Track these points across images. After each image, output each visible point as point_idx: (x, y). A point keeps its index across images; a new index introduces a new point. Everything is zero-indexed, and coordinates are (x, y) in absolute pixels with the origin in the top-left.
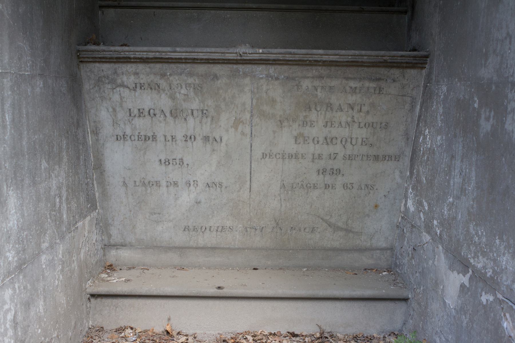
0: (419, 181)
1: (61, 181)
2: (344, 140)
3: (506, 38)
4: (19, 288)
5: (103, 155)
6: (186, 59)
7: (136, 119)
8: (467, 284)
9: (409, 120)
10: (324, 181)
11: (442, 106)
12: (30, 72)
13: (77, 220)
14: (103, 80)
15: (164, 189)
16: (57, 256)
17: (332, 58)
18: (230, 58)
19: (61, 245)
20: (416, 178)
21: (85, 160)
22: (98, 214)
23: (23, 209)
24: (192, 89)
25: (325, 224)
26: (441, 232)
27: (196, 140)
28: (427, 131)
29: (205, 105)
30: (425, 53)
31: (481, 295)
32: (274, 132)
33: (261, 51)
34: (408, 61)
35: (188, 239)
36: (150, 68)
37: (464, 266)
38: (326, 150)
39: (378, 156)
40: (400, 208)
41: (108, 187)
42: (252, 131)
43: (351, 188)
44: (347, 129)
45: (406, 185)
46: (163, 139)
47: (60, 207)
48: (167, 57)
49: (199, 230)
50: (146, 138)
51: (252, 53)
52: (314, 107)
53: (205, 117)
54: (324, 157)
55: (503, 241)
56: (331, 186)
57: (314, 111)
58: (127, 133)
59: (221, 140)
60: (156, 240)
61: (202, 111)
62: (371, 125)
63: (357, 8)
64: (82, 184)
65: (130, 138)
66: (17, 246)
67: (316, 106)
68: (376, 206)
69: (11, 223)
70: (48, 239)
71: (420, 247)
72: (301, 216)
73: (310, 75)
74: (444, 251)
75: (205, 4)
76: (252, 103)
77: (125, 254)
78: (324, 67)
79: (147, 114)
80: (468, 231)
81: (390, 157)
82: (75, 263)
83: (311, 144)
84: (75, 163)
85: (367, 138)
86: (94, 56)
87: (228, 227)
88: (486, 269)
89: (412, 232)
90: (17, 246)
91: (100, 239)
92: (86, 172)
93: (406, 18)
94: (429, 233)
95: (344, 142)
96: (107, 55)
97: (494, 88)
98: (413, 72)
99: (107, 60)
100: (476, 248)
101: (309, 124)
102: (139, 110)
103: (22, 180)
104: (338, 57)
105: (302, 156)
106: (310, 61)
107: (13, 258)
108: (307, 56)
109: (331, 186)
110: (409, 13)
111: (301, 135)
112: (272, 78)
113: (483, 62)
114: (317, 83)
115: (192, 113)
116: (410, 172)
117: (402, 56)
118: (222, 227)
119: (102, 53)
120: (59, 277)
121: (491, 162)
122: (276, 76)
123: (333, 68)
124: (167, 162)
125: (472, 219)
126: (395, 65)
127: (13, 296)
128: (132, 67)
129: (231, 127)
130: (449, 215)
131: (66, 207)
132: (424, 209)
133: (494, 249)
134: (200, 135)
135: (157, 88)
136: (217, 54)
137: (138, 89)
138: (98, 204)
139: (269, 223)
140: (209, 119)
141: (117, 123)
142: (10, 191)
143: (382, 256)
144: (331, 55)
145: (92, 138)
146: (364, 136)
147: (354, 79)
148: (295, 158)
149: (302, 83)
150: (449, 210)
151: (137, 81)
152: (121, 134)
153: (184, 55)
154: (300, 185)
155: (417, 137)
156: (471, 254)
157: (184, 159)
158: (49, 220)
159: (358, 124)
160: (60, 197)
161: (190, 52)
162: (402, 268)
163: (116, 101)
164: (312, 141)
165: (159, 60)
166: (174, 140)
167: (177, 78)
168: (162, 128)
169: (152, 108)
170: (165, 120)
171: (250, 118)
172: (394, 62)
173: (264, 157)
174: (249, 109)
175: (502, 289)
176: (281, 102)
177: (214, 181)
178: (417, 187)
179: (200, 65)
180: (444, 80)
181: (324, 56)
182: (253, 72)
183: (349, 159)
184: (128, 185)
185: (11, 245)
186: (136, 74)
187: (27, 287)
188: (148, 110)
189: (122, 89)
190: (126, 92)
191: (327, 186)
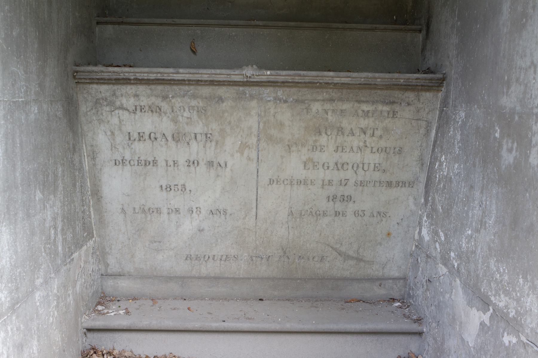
0: (434, 209)
1: (56, 211)
2: (355, 166)
3: (530, 67)
4: (12, 329)
5: (100, 180)
6: (189, 80)
7: (136, 143)
8: (487, 323)
9: (424, 145)
10: (334, 209)
11: (460, 132)
12: (24, 98)
13: (73, 251)
14: (101, 101)
15: (165, 216)
16: (51, 292)
17: (344, 80)
18: (235, 80)
19: (56, 280)
20: (431, 206)
21: (81, 186)
22: (95, 242)
23: (16, 245)
24: (195, 112)
25: (335, 253)
26: (458, 265)
27: (200, 165)
28: (443, 157)
29: (210, 129)
30: (441, 76)
31: (503, 337)
32: (282, 157)
33: (269, 73)
34: (423, 84)
35: (190, 268)
36: (151, 89)
37: (485, 303)
38: (337, 176)
39: (391, 182)
40: (414, 236)
41: (105, 214)
42: (258, 155)
43: (362, 215)
44: (359, 154)
45: (420, 212)
46: (164, 164)
47: (55, 239)
48: (169, 78)
49: (202, 259)
50: (147, 163)
51: (259, 75)
52: (324, 131)
53: (209, 141)
54: (334, 183)
55: (528, 281)
56: (341, 213)
57: (324, 134)
58: (126, 158)
59: (226, 165)
60: (155, 269)
61: (206, 134)
62: (384, 150)
63: (369, 26)
64: (78, 212)
65: (130, 162)
66: (10, 285)
67: (326, 130)
68: (389, 234)
69: (4, 261)
70: (42, 274)
71: (435, 279)
72: (310, 244)
73: (320, 97)
74: (462, 285)
75: (209, 21)
76: (259, 127)
77: (123, 284)
78: (335, 90)
79: (147, 137)
80: (488, 267)
81: (404, 183)
82: (71, 297)
83: (321, 169)
84: (70, 190)
85: (379, 164)
86: (92, 77)
87: (232, 256)
88: (508, 309)
89: (427, 262)
90: (10, 285)
91: (97, 268)
92: (82, 200)
93: (420, 37)
94: (445, 265)
95: (356, 167)
96: (106, 76)
97: (517, 118)
98: (428, 95)
99: (106, 82)
100: (498, 285)
101: (319, 148)
102: (139, 133)
103: (16, 214)
104: (350, 79)
105: (311, 182)
106: (320, 83)
107: (6, 298)
108: (317, 78)
109: (341, 213)
110: (424, 32)
111: (310, 160)
112: (280, 101)
113: (505, 90)
114: (328, 106)
115: (196, 137)
116: (424, 199)
117: (417, 79)
118: (227, 256)
119: (100, 74)
120: (54, 314)
121: (513, 196)
122: (284, 99)
123: (345, 91)
124: (169, 188)
125: (493, 254)
126: (410, 87)
127: (6, 339)
128: (131, 89)
129: (237, 152)
130: (468, 248)
131: (61, 238)
132: (440, 239)
133: (518, 289)
134: (203, 159)
135: (158, 111)
136: (222, 76)
137: (138, 112)
138: (95, 232)
139: (276, 252)
140: (214, 143)
141: (115, 147)
142: (3, 228)
143: (395, 286)
144: (343, 78)
145: (88, 163)
146: (377, 162)
147: (367, 102)
148: (304, 184)
149: (312, 106)
150: (468, 243)
151: (137, 103)
152: (120, 159)
153: (187, 77)
154: (308, 213)
155: (432, 164)
156: (491, 291)
157: (187, 185)
158: (43, 254)
159: (370, 149)
160: (55, 228)
161: (193, 74)
162: (416, 299)
163: (115, 124)
164: (321, 166)
165: (161, 82)
166: (176, 165)
167: (179, 100)
168: (163, 152)
169: (153, 131)
170: (166, 144)
171: (257, 142)
172: (409, 85)
173: (272, 183)
174: (256, 133)
175: (526, 331)
176: (289, 126)
177: (218, 208)
178: (432, 216)
179: (204, 87)
180: (461, 106)
181: (335, 79)
182: (260, 94)
183: (361, 186)
184: (127, 212)
185: (4, 285)
186: (136, 96)
187: (20, 328)
188: (148, 133)
189: (121, 112)
190: (125, 115)
191: (337, 214)
